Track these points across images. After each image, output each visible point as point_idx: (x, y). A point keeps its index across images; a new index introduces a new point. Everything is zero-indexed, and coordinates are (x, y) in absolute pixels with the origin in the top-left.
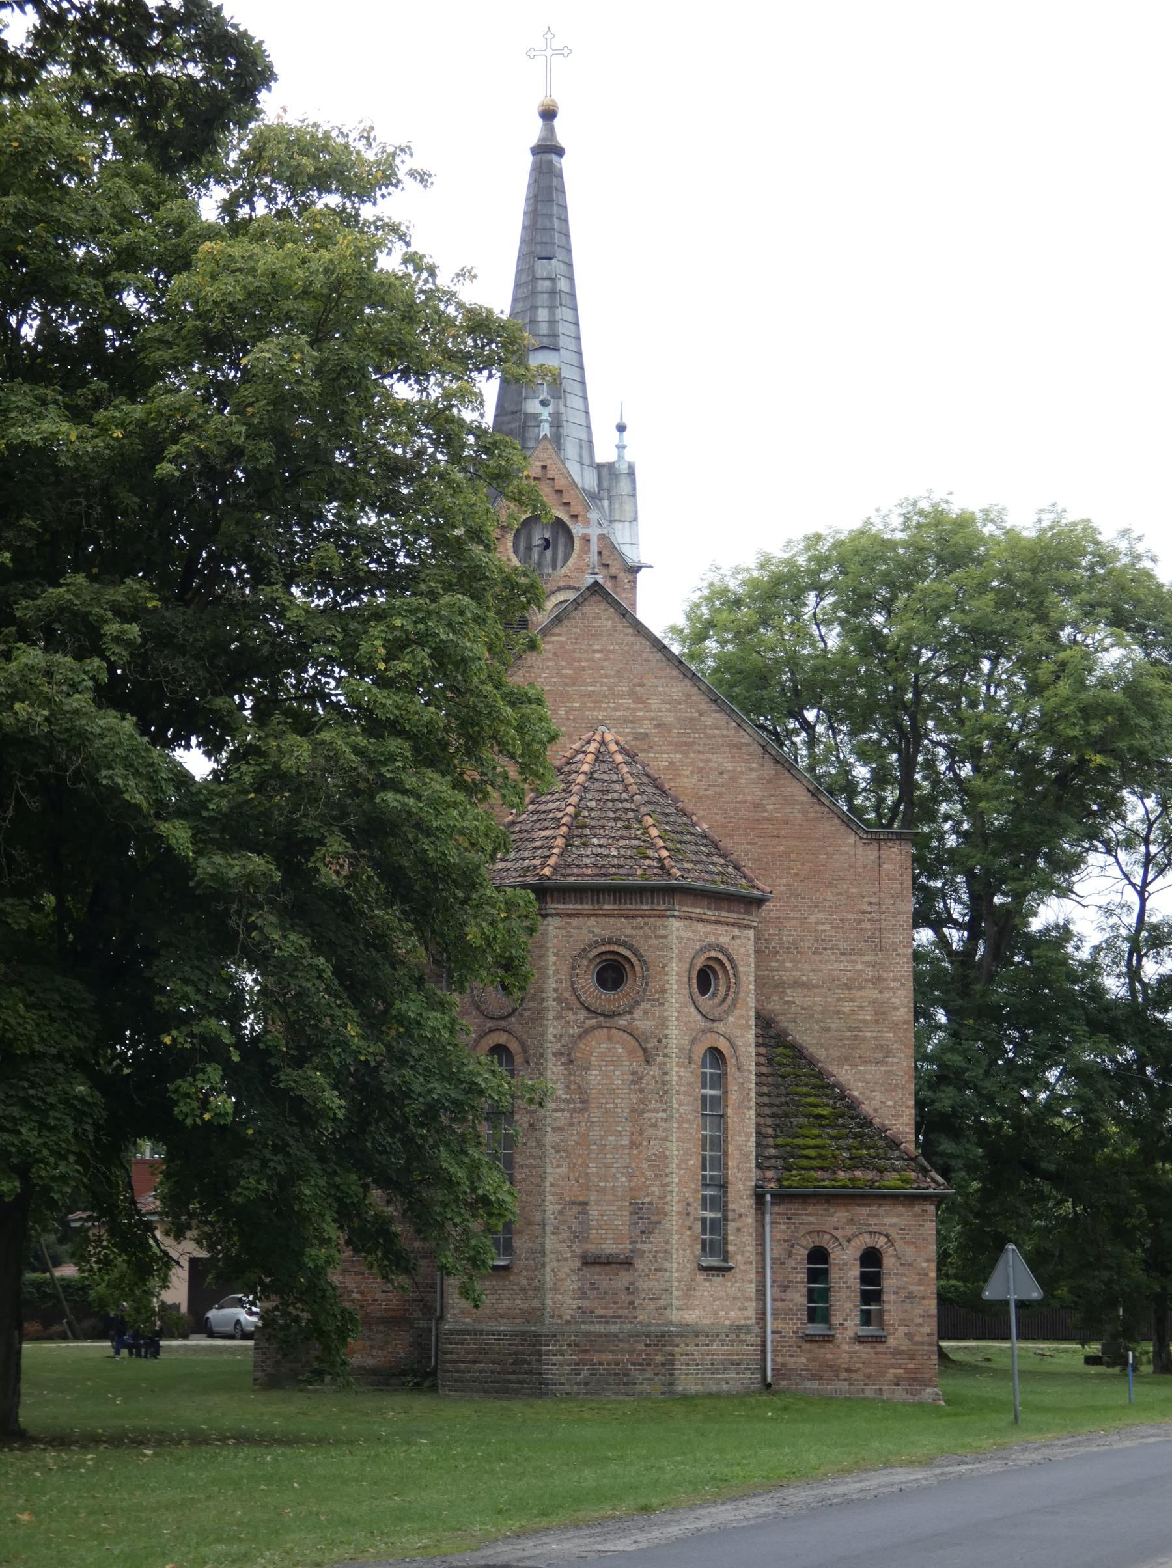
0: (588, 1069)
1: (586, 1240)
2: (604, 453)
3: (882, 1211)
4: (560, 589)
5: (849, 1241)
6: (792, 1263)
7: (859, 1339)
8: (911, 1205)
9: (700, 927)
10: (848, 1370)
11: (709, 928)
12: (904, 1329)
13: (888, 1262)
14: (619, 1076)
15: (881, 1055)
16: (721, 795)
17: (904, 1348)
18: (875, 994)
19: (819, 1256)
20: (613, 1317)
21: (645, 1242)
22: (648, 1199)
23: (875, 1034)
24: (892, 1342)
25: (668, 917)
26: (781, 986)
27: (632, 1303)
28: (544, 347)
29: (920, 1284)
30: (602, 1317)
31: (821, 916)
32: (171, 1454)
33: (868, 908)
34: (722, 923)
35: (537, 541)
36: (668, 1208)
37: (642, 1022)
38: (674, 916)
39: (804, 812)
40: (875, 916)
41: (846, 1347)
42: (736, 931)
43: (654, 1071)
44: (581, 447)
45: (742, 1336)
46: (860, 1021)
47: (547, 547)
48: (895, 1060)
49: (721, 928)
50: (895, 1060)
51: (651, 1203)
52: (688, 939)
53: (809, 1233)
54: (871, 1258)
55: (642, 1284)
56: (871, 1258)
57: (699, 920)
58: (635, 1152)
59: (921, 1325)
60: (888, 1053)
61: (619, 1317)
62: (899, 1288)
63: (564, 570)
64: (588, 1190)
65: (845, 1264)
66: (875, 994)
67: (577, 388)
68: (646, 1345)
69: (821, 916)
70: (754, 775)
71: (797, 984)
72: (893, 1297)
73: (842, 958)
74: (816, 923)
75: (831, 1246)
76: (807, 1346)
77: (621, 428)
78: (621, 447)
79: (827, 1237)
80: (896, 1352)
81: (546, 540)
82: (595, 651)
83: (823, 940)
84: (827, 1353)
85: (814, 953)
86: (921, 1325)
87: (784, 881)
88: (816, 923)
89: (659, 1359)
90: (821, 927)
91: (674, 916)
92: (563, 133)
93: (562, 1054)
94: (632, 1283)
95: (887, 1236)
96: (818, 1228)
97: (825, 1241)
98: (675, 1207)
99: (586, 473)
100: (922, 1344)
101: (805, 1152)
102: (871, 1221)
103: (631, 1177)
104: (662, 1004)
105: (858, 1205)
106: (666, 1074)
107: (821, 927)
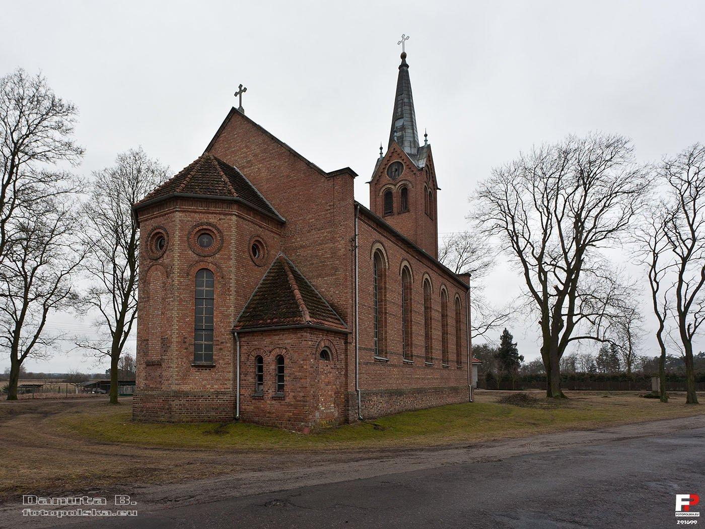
0: (150, 284)
1: (148, 355)
2: (422, 144)
3: (284, 337)
4: (400, 181)
5: (270, 352)
6: (248, 363)
7: (273, 398)
8: (296, 333)
9: (197, 216)
10: (269, 413)
11: (202, 216)
12: (292, 394)
13: (286, 361)
14: (159, 284)
15: (334, 271)
16: (275, 176)
17: (293, 403)
18: (332, 245)
19: (260, 359)
20: (155, 388)
21: (165, 355)
22: (166, 336)
23: (331, 263)
24: (287, 400)
25: (174, 212)
26: (295, 249)
27: (161, 382)
28: (399, 119)
29: (299, 372)
30: (152, 388)
31: (310, 216)
32: (702, 374)
33: (329, 208)
34: (210, 213)
35: (394, 170)
36: (173, 340)
37: (166, 260)
38: (177, 211)
39: (304, 173)
40: (332, 211)
41: (268, 402)
42: (222, 217)
43: (170, 280)
44: (410, 143)
45: (219, 397)
46: (325, 258)
47: (396, 171)
48: (339, 273)
49: (210, 216)
50: (339, 273)
51: (167, 338)
52: (188, 221)
53: (255, 349)
54: (280, 360)
55: (164, 374)
56: (280, 360)
57: (195, 212)
58: (163, 316)
59: (300, 392)
60: (336, 269)
61: (157, 388)
62: (291, 374)
63: (401, 176)
64: (148, 334)
65: (269, 363)
66: (332, 245)
67: (410, 131)
68: (163, 400)
69: (310, 216)
70: (286, 164)
71: (302, 247)
72: (288, 378)
73: (319, 232)
74: (309, 220)
75: (263, 355)
76: (254, 401)
77: (426, 135)
78: (426, 141)
79: (262, 351)
80: (289, 405)
81: (396, 169)
82: (236, 134)
83: (312, 226)
84: (261, 405)
85: (308, 233)
86: (300, 392)
87: (297, 205)
88: (309, 220)
89: (167, 407)
90: (311, 221)
91: (177, 211)
92: (408, 61)
93: (142, 279)
94: (161, 374)
95: (286, 349)
96: (258, 347)
97: (261, 353)
98: (175, 340)
99: (412, 150)
100: (300, 401)
101: (115, 302)
102: (280, 342)
103: (161, 327)
104: (173, 251)
105: (275, 335)
106: (173, 281)
107: (311, 221)
